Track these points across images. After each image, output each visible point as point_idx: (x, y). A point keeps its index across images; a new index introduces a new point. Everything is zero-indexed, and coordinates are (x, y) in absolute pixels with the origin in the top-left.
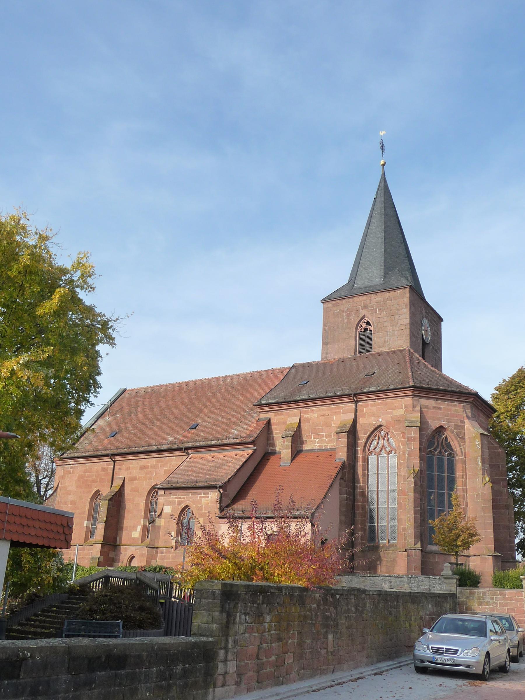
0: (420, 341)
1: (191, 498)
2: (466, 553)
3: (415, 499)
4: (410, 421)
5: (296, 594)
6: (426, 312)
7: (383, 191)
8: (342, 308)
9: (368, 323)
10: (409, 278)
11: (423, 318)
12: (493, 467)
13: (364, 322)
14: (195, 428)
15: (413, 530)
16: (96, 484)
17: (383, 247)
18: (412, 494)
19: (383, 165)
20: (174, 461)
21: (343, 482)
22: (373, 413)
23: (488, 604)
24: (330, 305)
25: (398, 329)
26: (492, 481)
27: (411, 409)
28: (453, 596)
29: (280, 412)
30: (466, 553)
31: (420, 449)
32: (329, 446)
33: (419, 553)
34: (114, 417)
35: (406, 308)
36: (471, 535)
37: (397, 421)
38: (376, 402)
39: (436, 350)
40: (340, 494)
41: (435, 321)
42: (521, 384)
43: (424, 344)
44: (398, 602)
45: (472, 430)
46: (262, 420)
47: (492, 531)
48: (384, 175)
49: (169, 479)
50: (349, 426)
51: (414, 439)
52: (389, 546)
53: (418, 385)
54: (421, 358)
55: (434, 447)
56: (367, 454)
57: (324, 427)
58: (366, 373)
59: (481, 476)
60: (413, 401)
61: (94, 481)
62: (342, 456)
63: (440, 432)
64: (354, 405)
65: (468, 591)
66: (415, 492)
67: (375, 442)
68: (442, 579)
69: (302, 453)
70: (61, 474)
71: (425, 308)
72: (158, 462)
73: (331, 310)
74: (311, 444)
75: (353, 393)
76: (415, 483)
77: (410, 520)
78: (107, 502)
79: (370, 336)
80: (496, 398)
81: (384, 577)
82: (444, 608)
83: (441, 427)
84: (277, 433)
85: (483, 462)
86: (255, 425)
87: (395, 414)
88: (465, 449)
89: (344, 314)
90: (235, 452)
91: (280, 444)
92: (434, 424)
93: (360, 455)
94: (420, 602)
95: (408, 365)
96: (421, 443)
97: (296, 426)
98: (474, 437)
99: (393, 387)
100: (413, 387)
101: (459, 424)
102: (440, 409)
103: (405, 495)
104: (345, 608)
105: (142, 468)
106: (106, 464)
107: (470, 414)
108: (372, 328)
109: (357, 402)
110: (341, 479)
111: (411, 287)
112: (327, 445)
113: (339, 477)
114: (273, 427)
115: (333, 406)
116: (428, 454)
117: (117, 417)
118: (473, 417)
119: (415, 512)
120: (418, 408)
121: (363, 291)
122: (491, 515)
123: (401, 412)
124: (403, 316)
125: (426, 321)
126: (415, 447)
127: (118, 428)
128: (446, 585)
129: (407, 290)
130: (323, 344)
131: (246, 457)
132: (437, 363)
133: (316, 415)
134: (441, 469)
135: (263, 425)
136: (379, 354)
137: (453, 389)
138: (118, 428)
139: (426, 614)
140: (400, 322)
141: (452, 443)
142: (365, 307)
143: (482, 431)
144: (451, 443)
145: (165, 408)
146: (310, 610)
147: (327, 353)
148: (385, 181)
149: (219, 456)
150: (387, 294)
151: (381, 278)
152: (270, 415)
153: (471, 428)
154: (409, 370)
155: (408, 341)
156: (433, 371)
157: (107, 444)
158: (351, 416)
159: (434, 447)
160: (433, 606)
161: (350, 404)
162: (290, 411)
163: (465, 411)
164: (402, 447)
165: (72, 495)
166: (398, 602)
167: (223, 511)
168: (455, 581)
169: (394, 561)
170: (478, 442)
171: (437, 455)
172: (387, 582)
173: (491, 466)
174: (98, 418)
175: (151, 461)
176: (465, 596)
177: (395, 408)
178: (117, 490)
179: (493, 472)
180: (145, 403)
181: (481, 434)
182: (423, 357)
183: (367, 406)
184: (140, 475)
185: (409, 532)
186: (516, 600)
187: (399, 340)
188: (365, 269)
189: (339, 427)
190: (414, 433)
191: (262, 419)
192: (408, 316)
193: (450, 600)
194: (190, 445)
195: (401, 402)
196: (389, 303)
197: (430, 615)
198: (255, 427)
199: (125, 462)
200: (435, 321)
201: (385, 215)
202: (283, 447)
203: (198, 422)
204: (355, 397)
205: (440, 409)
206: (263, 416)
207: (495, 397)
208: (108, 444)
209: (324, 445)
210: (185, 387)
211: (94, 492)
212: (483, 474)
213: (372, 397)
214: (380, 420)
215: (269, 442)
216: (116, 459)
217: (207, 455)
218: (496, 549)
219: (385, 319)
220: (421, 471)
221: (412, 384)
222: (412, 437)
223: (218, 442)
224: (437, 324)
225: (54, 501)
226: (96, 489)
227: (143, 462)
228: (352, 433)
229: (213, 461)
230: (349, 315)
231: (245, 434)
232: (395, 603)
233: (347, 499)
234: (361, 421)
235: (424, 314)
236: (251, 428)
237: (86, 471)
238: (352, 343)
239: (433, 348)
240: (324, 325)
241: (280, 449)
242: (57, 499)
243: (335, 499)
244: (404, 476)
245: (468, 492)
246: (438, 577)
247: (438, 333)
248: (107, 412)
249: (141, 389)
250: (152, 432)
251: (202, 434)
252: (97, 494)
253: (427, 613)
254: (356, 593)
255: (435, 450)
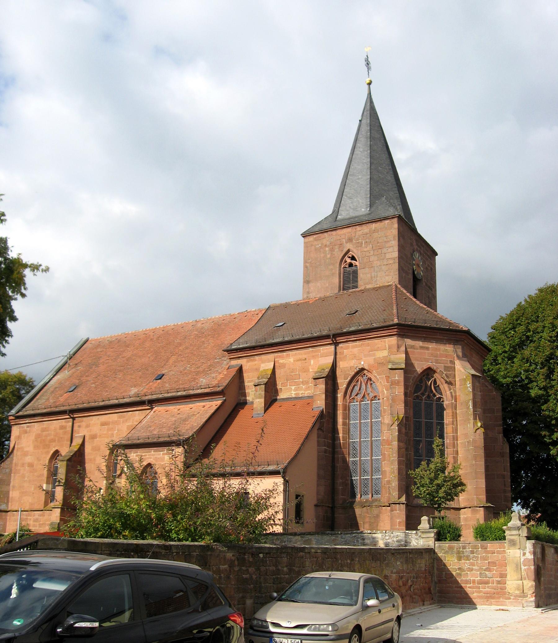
0: (411, 277)
1: (153, 455)
2: (452, 504)
3: (399, 448)
4: (394, 363)
5: (195, 554)
6: (417, 245)
7: (369, 112)
8: (324, 241)
9: (353, 258)
10: (398, 208)
11: (414, 252)
12: (482, 409)
13: (349, 257)
14: (160, 379)
15: (397, 483)
16: (54, 444)
17: (369, 173)
18: (395, 443)
19: (369, 84)
20: (135, 417)
21: (320, 432)
22: (354, 356)
23: (468, 558)
24: (311, 239)
25: (385, 263)
26: (484, 426)
27: (395, 350)
28: (430, 551)
29: (252, 358)
30: (452, 504)
31: (406, 394)
32: (307, 393)
33: (403, 507)
34: (74, 370)
35: (394, 240)
36: (455, 486)
37: (381, 364)
38: (358, 343)
39: (429, 287)
40: (318, 445)
41: (428, 255)
42: (519, 322)
43: (416, 280)
44: (352, 560)
45: (463, 370)
46: (233, 367)
47: (484, 480)
48: (370, 94)
49: (130, 435)
50: (327, 370)
51: (398, 383)
52: (373, 501)
53: (403, 323)
54: (412, 297)
55: (422, 391)
56: (348, 401)
57: (300, 374)
58: (348, 312)
59: (472, 421)
60: (398, 341)
61: (53, 441)
62: (320, 403)
63: (428, 375)
64: (333, 347)
65: (447, 545)
66: (399, 440)
67: (357, 388)
68: (420, 534)
69: (276, 403)
70: (18, 434)
71: (416, 241)
72: (119, 417)
73: (312, 245)
74: (286, 392)
75: (331, 333)
76: (399, 431)
77: (393, 472)
78: (65, 462)
79: (355, 273)
80: (493, 338)
81: (356, 534)
82: (418, 566)
83: (429, 369)
84: (249, 380)
85: (474, 406)
86: (225, 373)
87: (378, 356)
88: (455, 392)
89: (327, 249)
90: (203, 404)
91: (253, 393)
92: (419, 367)
93: (340, 402)
94: (385, 560)
95: (394, 301)
96: (406, 387)
97: (270, 372)
98: (465, 379)
99: (375, 325)
100: (397, 325)
101: (449, 365)
102: (427, 348)
103: (389, 445)
104: (272, 568)
105: (103, 424)
106: (65, 423)
107: (460, 354)
108: (357, 263)
109: (336, 344)
110: (319, 429)
111: (399, 217)
112: (304, 392)
113: (317, 427)
114: (245, 375)
115: (310, 349)
116: (415, 399)
117: (78, 370)
118: (465, 356)
119: (400, 463)
120: (403, 348)
121: (347, 222)
122: (482, 463)
123: (385, 353)
124: (390, 250)
125: (417, 255)
126: (400, 391)
127: (77, 381)
128: (424, 540)
129: (396, 220)
130: (304, 282)
131: (216, 408)
132: (431, 302)
133: (292, 360)
134: (429, 415)
135: (233, 372)
136: (363, 291)
137: (442, 327)
138: (77, 381)
139: (392, 572)
140: (388, 256)
141: (441, 387)
142: (350, 240)
143: (473, 372)
144: (440, 386)
145: (129, 358)
146: (219, 571)
147: (308, 293)
148: (371, 102)
149: (185, 408)
150: (374, 226)
151: (367, 208)
152: (242, 362)
153: (461, 369)
154: (395, 307)
155: (397, 276)
156: (422, 307)
157: (66, 401)
158: (330, 360)
159: (422, 391)
160: (402, 563)
161: (328, 347)
162: (264, 357)
163: (456, 351)
164: (385, 392)
165: (29, 457)
166: (352, 560)
167: (188, 467)
168: (432, 535)
169: (377, 517)
170: (469, 385)
171: (426, 400)
172: (359, 540)
173: (484, 411)
174: (57, 372)
175: (112, 417)
176: (443, 551)
177: (378, 349)
178: (76, 450)
179: (487, 416)
180: (108, 354)
181: (472, 375)
182: (415, 296)
183: (347, 348)
184: (100, 433)
185: (393, 485)
186: (498, 552)
187: (387, 275)
188: (350, 198)
189: (316, 373)
190: (399, 376)
191: (233, 366)
192: (396, 248)
193: (426, 556)
194: (154, 397)
195: (385, 342)
196: (375, 235)
197: (398, 572)
198: (225, 375)
199: (84, 419)
200: (428, 255)
201: (372, 138)
202: (255, 397)
203: (163, 372)
204: (335, 338)
205: (427, 348)
206: (234, 362)
207: (492, 337)
208: (66, 400)
209: (301, 393)
210: (151, 334)
211: (52, 452)
212: (475, 419)
213: (353, 338)
214: (362, 363)
215: (240, 392)
216: (75, 416)
217: (173, 408)
218: (488, 500)
219: (372, 253)
220: (406, 417)
221: (396, 321)
222: (395, 380)
223: (184, 393)
224: (430, 258)
225: (11, 463)
226: (54, 450)
227: (104, 418)
228: (331, 378)
229: (179, 414)
230: (332, 250)
231: (215, 382)
232: (349, 561)
233: (325, 451)
234: (341, 365)
235: (416, 247)
236: (222, 376)
237: (43, 430)
238: (336, 280)
239: (426, 284)
240: (305, 262)
241: (253, 399)
242: (14, 462)
243: (312, 452)
244: (388, 424)
245: (459, 439)
246: (414, 532)
247: (431, 269)
248: (67, 366)
249: (104, 339)
250: (114, 385)
251: (167, 385)
252: (56, 454)
253: (395, 571)
254: (290, 551)
255: (423, 394)
